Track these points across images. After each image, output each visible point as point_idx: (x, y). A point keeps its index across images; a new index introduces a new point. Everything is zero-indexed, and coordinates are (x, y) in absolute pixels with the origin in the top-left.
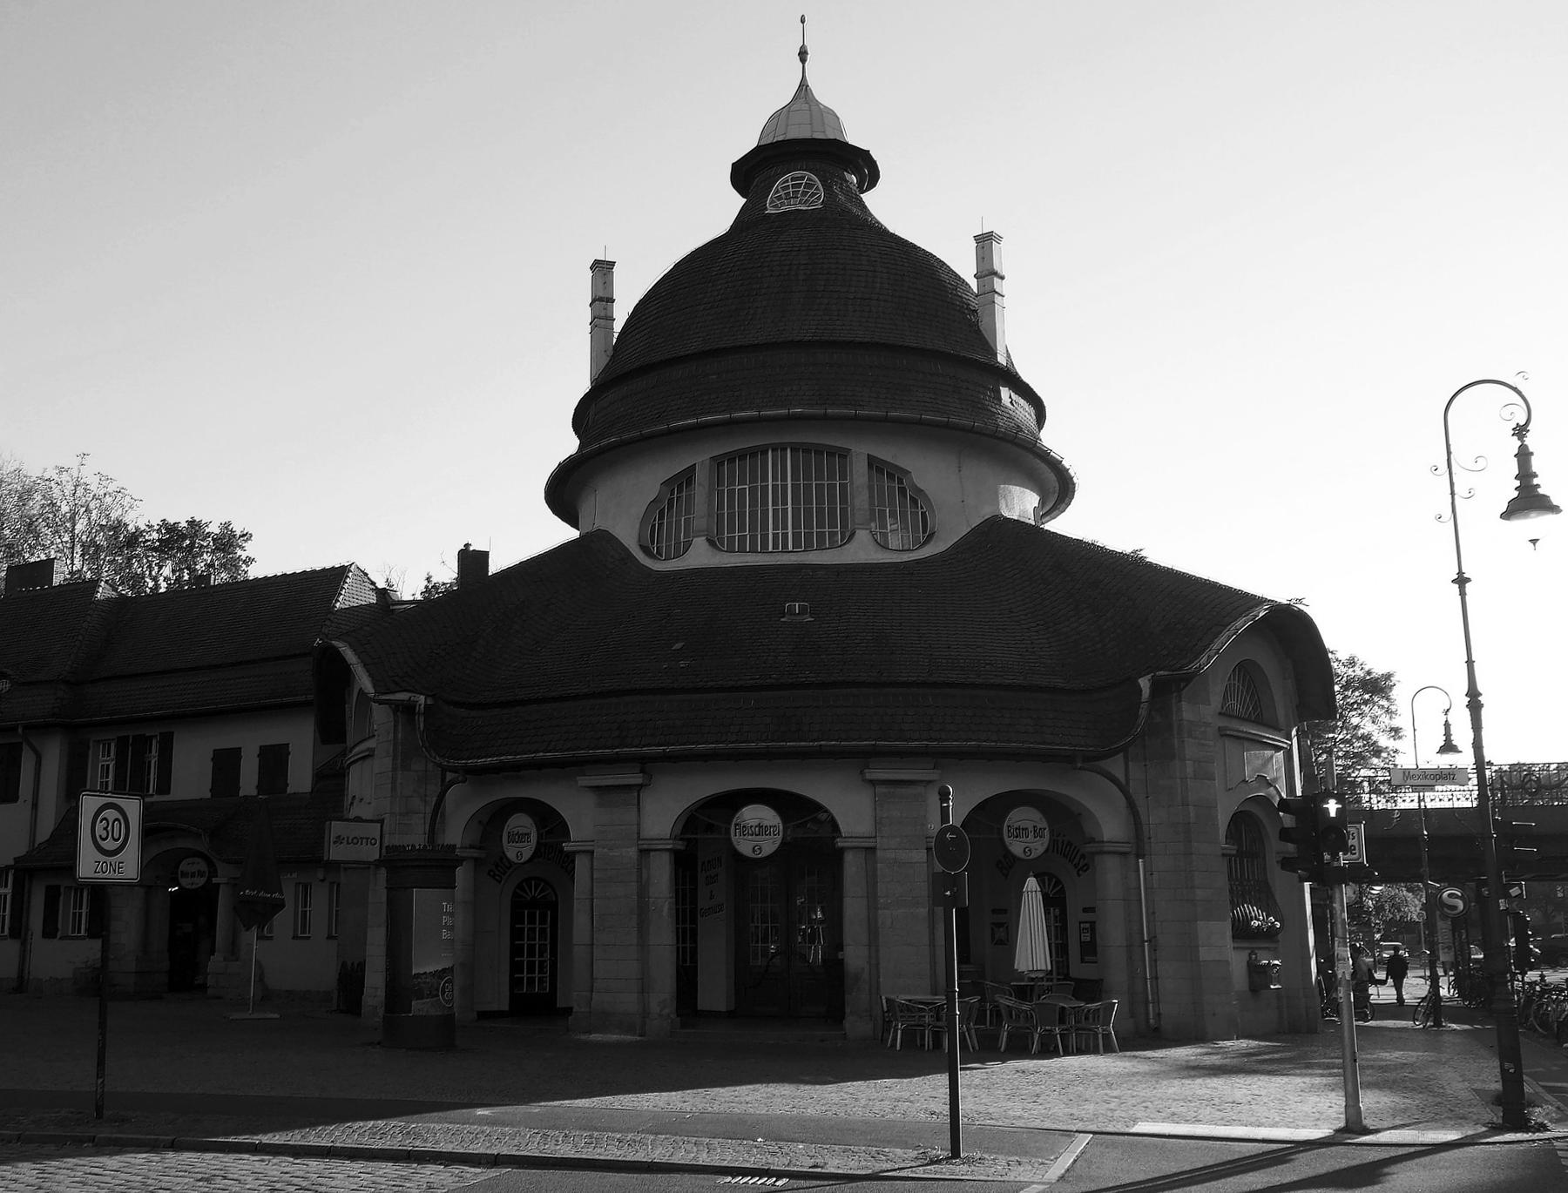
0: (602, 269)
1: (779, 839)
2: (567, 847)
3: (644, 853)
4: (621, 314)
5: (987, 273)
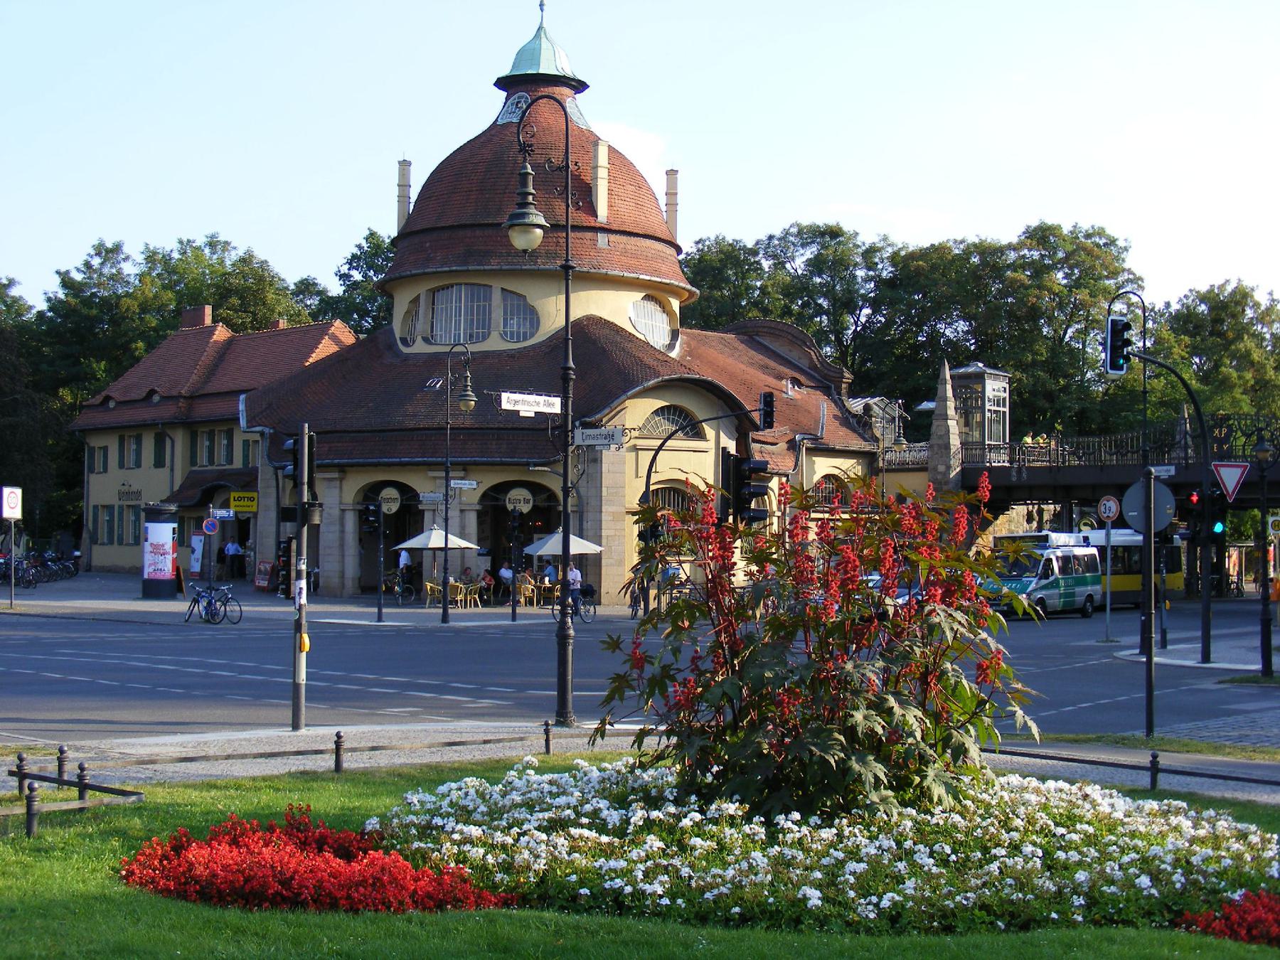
0: (405, 165)
1: (509, 496)
2: (420, 507)
3: (462, 511)
4: (414, 194)
5: (672, 194)
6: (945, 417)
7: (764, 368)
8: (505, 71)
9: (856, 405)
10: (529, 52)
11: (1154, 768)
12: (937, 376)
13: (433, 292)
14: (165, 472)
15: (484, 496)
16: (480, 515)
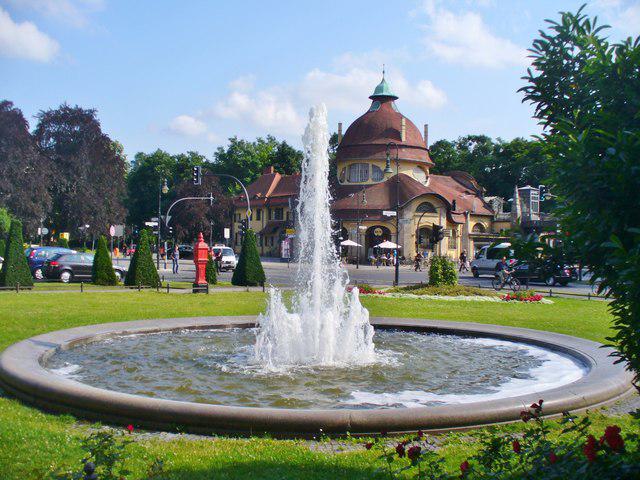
0: (340, 125)
5: (426, 132)
6: (516, 204)
7: (457, 188)
8: (372, 94)
9: (487, 199)
10: (379, 88)
11: (551, 292)
12: (514, 192)
13: (350, 166)
14: (260, 222)
15: (368, 230)
16: (366, 237)
